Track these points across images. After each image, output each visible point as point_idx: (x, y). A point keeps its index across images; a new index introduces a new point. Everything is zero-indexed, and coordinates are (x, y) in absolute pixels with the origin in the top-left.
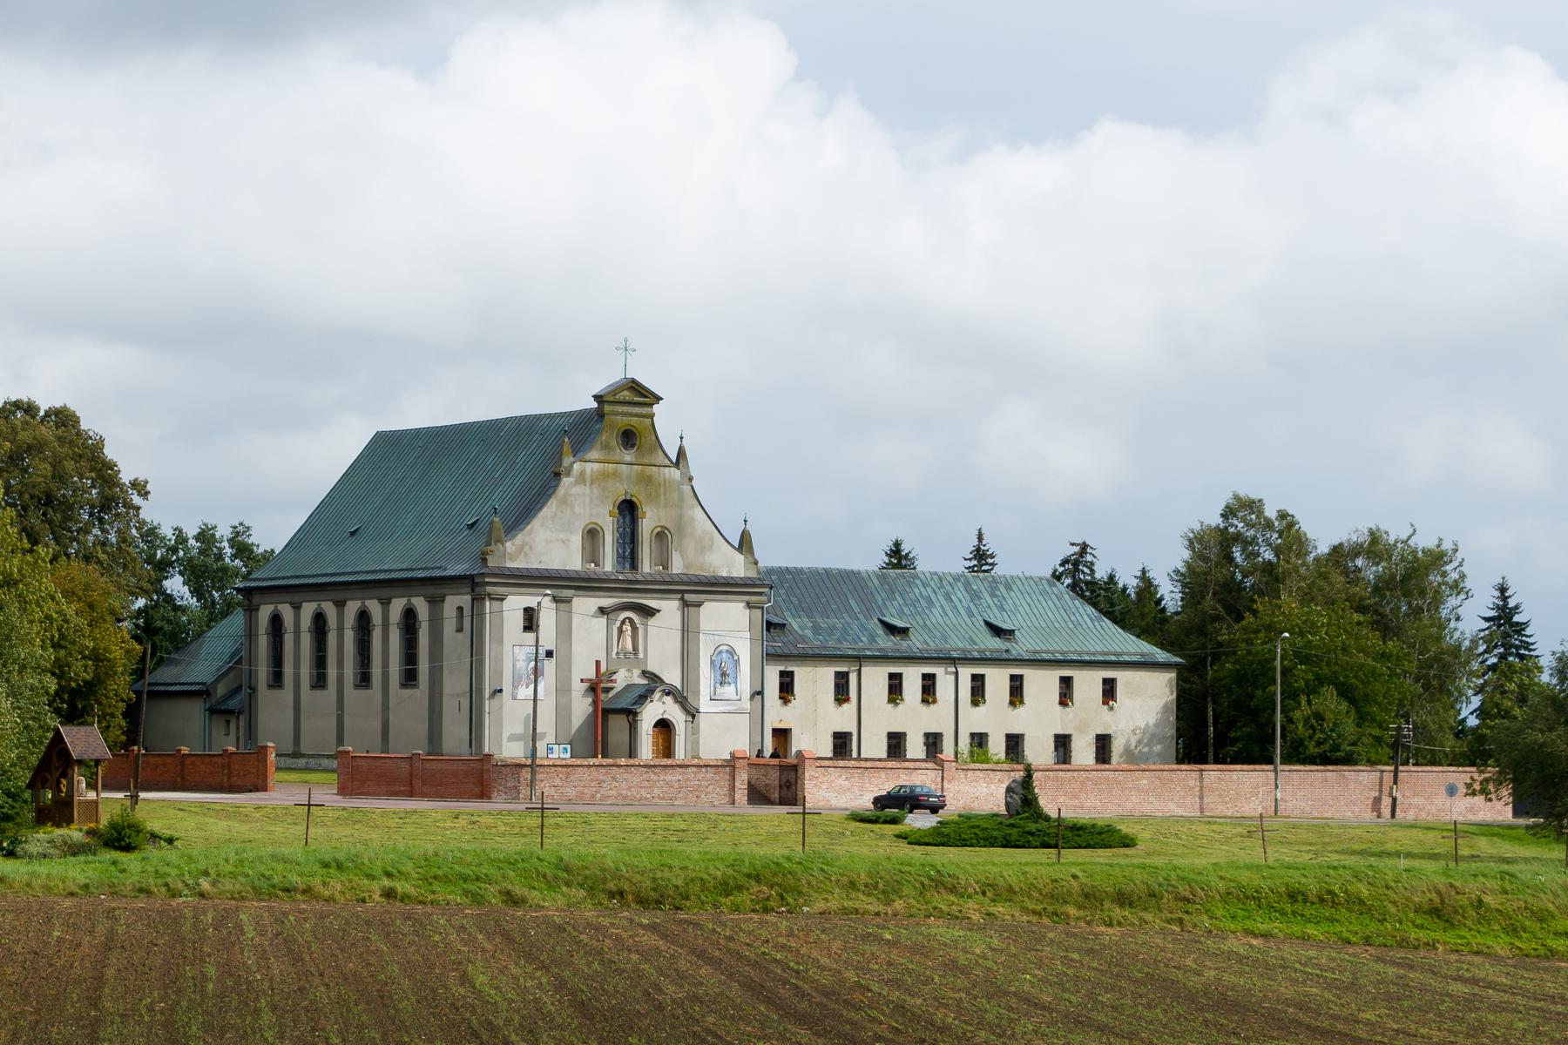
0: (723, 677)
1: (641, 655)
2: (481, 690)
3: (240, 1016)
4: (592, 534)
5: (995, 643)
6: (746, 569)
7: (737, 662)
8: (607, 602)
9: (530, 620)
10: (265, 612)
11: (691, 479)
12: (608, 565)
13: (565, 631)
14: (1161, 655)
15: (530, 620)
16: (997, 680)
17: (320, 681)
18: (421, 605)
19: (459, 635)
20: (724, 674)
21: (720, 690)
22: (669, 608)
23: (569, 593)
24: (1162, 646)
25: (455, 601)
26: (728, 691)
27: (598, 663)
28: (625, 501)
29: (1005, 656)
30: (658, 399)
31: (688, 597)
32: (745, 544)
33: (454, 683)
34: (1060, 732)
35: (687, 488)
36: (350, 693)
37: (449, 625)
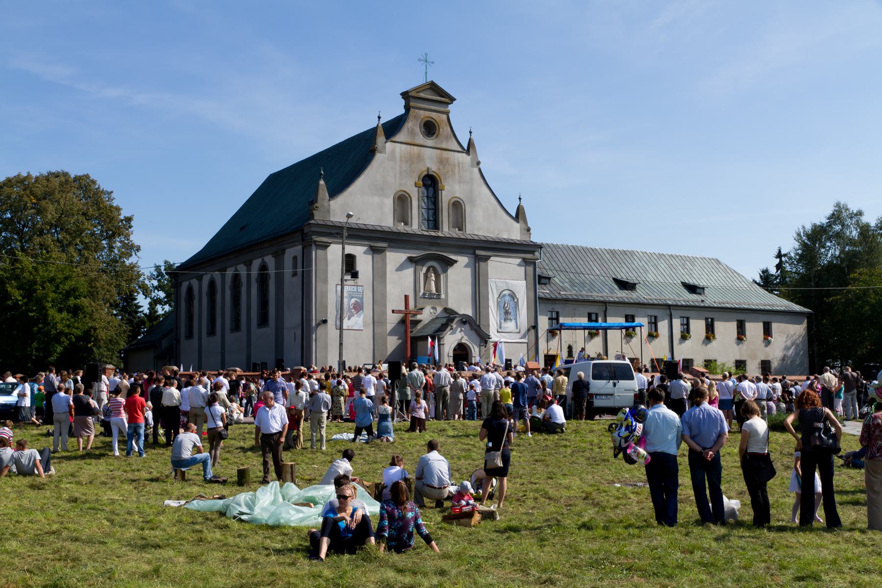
0: (506, 315)
1: (443, 296)
2: (309, 320)
3: (401, 439)
4: (402, 200)
5: (693, 299)
6: (521, 234)
7: (517, 304)
8: (415, 254)
9: (350, 265)
10: (185, 285)
11: (478, 163)
12: (416, 226)
13: (379, 276)
14: (797, 308)
15: (350, 265)
16: (698, 326)
17: (212, 332)
18: (270, 260)
19: (295, 279)
20: (507, 313)
21: (504, 325)
22: (462, 260)
23: (384, 245)
24: (796, 303)
25: (293, 251)
26: (510, 325)
27: (406, 297)
28: (426, 176)
29: (702, 305)
30: (453, 99)
31: (479, 252)
32: (519, 215)
33: (292, 318)
34: (738, 358)
35: (476, 170)
36: (230, 337)
37: (288, 270)
